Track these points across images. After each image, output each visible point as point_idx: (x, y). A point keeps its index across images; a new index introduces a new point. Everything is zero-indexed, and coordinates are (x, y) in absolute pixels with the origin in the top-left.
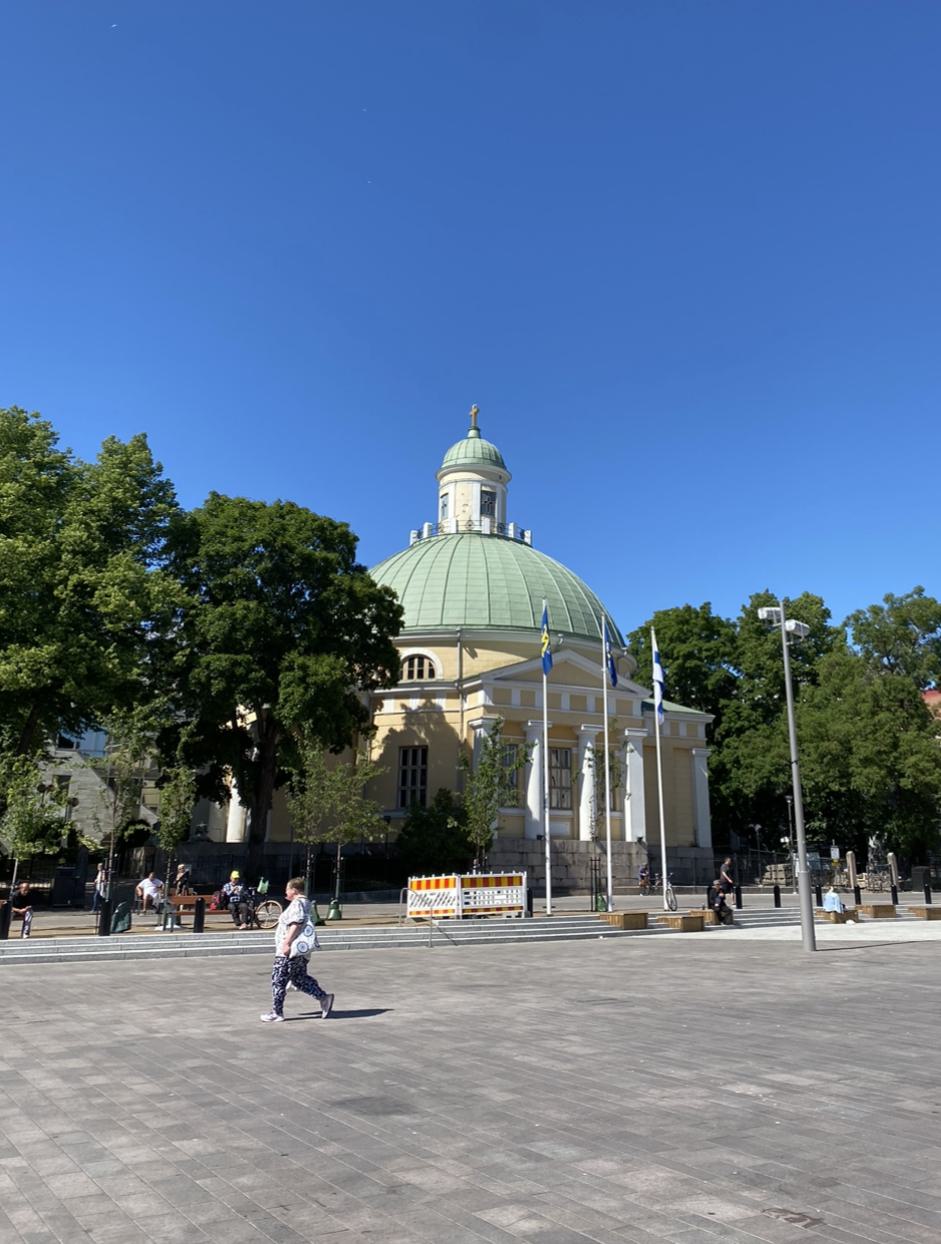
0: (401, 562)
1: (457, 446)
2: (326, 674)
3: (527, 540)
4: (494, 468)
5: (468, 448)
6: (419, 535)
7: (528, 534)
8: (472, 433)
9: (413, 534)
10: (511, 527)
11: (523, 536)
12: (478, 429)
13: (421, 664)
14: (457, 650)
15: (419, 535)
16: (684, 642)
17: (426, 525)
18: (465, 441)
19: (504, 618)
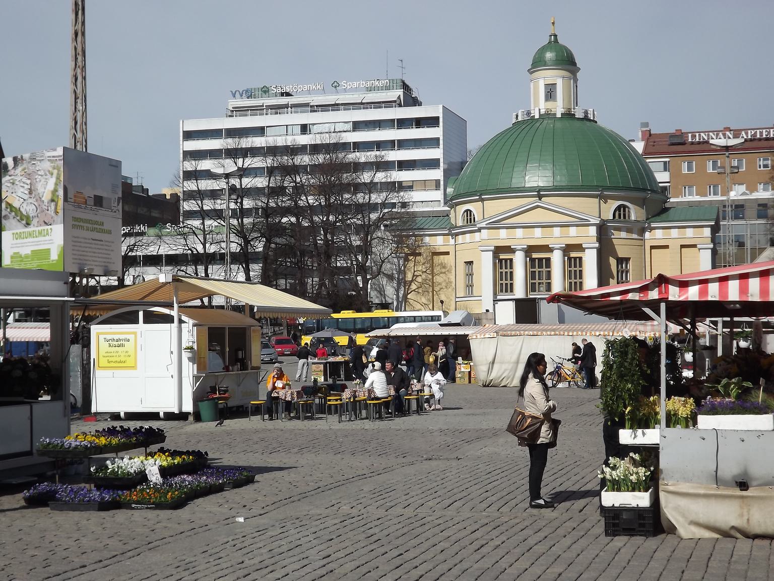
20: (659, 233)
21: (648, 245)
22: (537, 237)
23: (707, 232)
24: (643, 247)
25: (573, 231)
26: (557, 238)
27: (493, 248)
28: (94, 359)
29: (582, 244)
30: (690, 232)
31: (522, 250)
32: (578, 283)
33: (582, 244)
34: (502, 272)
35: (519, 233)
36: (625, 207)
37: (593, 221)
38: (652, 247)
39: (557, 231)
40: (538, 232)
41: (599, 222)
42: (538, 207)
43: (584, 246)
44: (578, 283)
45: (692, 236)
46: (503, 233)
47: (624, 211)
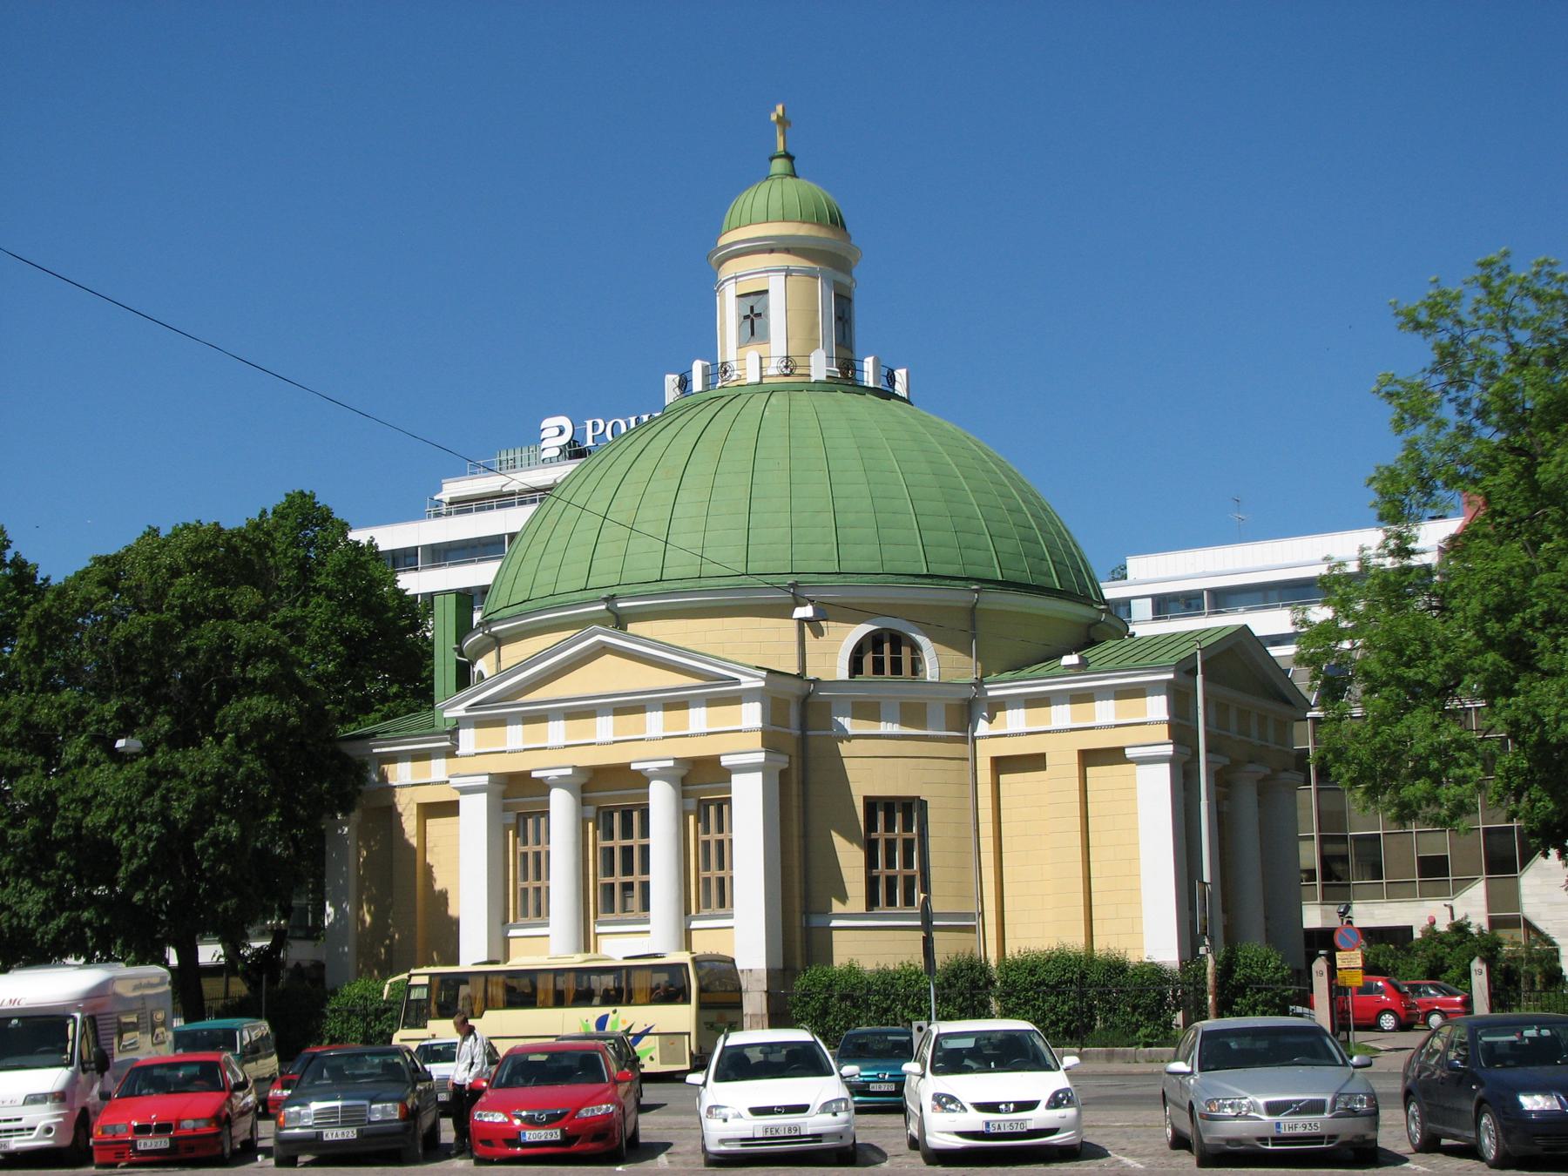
0: (646, 463)
1: (751, 191)
2: (1445, 451)
3: (900, 389)
4: (830, 255)
5: (764, 213)
6: (684, 384)
7: (901, 375)
8: (779, 166)
9: (671, 380)
10: (868, 364)
11: (891, 379)
12: (789, 157)
13: (896, 649)
14: (223, 979)
15: (684, 384)
16: (1495, 473)
17: (697, 367)
18: (766, 185)
19: (862, 557)
20: (1014, 720)
21: (986, 752)
22: (605, 741)
23: (1157, 707)
24: (970, 764)
25: (698, 718)
26: (652, 743)
27: (484, 780)
28: (757, 1111)
29: (1123, 749)
30: (1105, 711)
31: (662, 774)
32: (531, 891)
33: (1123, 749)
34: (612, 849)
35: (556, 732)
36: (897, 640)
37: (748, 683)
38: (1002, 765)
39: (655, 722)
40: (605, 727)
41: (762, 684)
42: (603, 649)
43: (1129, 753)
44: (531, 891)
45: (563, 742)
46: (515, 736)
47: (896, 649)
